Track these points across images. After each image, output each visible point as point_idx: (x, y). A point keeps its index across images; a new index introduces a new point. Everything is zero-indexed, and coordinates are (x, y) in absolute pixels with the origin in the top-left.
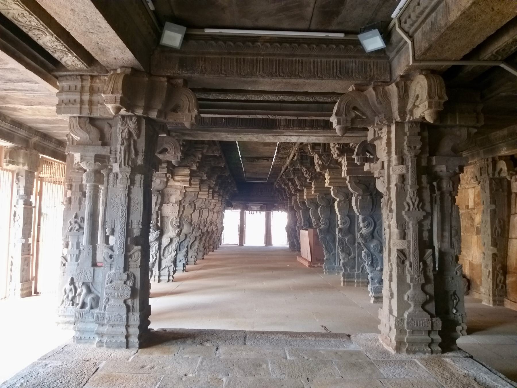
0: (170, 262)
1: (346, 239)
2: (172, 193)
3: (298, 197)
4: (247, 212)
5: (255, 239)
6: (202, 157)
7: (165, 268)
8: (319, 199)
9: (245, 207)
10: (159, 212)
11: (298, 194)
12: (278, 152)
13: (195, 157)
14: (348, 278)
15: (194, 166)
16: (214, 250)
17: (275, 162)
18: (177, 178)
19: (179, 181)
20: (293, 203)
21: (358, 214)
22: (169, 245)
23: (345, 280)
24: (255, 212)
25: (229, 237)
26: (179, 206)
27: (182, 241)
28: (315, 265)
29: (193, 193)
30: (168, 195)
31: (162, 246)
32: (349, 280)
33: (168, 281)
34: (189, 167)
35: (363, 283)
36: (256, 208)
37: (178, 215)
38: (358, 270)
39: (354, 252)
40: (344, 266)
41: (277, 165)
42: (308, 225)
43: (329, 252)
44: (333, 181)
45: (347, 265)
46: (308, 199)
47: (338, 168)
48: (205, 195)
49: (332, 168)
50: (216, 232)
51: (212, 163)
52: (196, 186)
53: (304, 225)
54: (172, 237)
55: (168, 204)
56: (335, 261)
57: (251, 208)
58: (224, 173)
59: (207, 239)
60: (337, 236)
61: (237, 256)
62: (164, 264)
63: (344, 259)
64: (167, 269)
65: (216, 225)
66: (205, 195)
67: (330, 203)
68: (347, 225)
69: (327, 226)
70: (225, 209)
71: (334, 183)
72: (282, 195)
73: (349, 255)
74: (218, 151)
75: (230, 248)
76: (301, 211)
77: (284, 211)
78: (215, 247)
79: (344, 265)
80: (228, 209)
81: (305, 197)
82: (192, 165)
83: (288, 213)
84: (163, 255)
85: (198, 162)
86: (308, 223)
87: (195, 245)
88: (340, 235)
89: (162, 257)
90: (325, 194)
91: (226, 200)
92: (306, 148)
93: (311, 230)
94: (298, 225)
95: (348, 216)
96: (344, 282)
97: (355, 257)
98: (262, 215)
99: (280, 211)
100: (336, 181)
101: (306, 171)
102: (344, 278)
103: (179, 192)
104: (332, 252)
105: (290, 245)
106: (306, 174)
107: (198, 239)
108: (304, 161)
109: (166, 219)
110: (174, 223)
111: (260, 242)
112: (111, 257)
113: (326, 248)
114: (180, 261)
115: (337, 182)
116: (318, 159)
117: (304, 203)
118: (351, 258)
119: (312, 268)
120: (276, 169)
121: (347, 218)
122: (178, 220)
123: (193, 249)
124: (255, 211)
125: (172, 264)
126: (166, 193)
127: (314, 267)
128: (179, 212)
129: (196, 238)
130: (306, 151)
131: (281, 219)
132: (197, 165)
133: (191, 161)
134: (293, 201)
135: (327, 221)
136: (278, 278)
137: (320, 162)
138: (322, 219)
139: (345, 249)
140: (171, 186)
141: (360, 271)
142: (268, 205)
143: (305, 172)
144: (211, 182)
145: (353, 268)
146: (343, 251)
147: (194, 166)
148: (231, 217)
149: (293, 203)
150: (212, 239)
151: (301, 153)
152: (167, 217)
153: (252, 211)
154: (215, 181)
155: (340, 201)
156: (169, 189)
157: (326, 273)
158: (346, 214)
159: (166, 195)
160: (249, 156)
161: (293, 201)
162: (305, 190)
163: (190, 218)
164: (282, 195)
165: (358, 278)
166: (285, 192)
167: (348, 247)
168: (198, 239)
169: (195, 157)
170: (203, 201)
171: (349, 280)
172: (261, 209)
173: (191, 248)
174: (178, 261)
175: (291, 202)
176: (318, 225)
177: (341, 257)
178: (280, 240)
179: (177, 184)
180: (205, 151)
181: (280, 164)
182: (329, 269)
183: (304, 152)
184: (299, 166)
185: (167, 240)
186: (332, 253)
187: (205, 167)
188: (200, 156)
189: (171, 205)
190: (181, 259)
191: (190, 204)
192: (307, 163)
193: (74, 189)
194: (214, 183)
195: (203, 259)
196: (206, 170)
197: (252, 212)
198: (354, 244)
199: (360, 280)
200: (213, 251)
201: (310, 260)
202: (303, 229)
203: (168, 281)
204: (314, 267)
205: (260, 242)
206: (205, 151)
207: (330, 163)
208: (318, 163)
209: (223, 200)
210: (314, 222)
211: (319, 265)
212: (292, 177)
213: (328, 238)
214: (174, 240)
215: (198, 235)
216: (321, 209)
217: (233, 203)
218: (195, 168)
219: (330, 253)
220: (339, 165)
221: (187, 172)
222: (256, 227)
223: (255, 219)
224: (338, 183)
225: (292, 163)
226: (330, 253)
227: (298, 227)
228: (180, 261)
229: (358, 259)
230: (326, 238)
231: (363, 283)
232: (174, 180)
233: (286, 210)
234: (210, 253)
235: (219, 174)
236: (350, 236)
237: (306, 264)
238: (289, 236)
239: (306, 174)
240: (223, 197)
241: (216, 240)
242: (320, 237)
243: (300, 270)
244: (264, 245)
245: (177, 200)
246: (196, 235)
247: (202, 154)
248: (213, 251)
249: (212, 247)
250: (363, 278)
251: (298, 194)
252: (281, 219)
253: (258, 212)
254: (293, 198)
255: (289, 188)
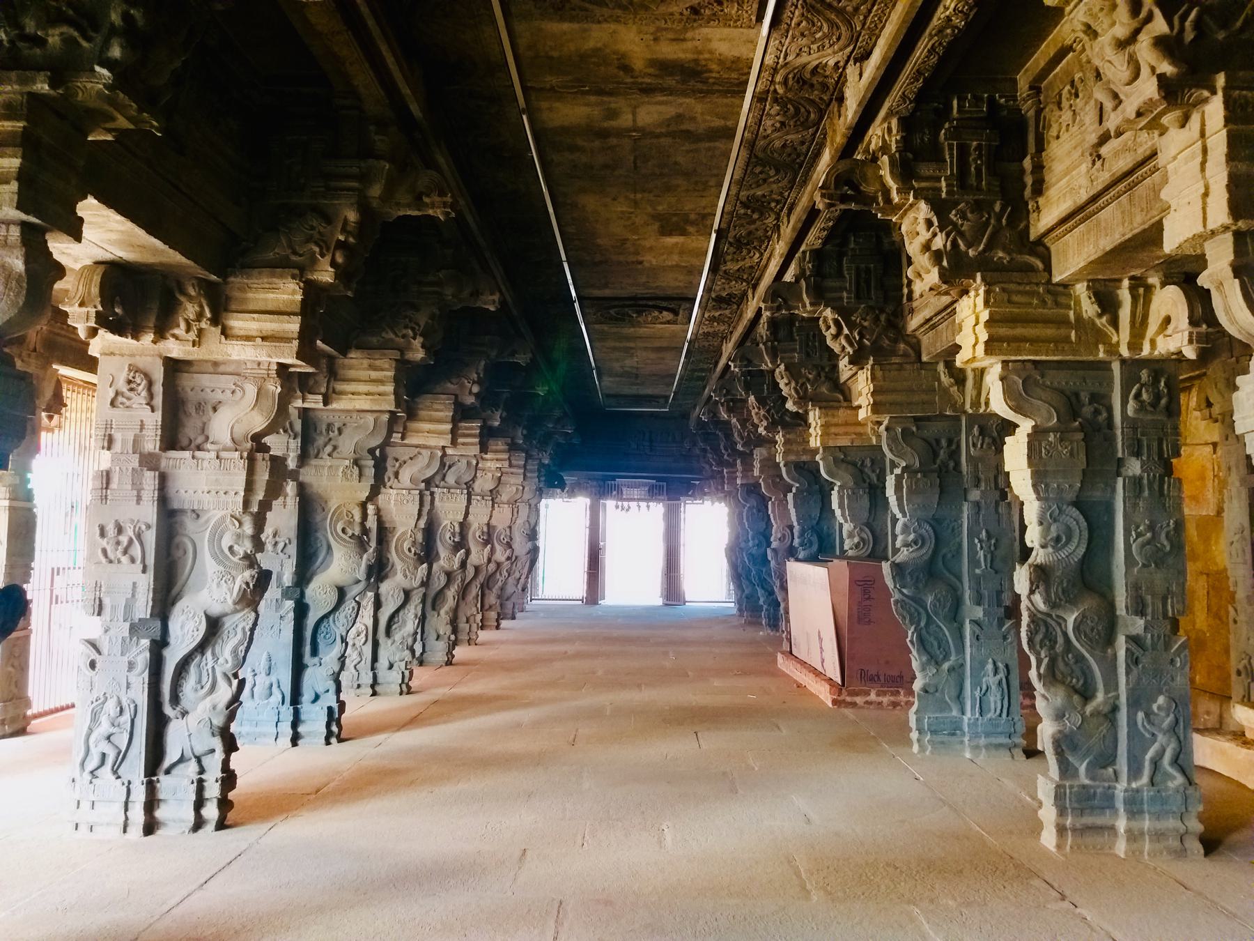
0: (206, 732)
1: (1071, 619)
2: (218, 396)
3: (780, 448)
4: (610, 504)
5: (633, 585)
6: (361, 224)
7: (182, 760)
8: (892, 440)
9: (603, 489)
10: (371, 508)
11: (779, 438)
12: (714, 269)
13: (328, 219)
14: (1082, 812)
15: (325, 263)
16: (504, 623)
17: (699, 324)
18: (238, 323)
19: (248, 338)
20: (756, 473)
21: (842, 521)
22: (201, 647)
23: (1069, 822)
24: (633, 504)
25: (558, 577)
26: (251, 461)
27: (326, 616)
28: (859, 700)
29: (370, 419)
30: (199, 407)
31: (167, 653)
32: (1088, 820)
33: (401, 694)
34: (301, 271)
35: (1158, 836)
36: (636, 493)
37: (246, 504)
38: (1135, 772)
39: (1111, 684)
40: (1059, 753)
41: (707, 335)
42: (815, 547)
43: (934, 660)
44: (1003, 331)
45: (1074, 748)
46: (825, 448)
47: (1031, 269)
48: (441, 433)
49: (999, 268)
50: (506, 565)
51: (449, 291)
52: (381, 388)
53: (801, 545)
54: (216, 610)
55: (199, 448)
56: (959, 697)
57: (620, 492)
58: (513, 354)
59: (476, 590)
60: (1024, 603)
61: (570, 648)
62: (177, 740)
63: (1059, 716)
64: (192, 767)
65: (509, 545)
66: (441, 433)
67: (935, 454)
68: (1076, 549)
69: (927, 551)
70: (540, 493)
71: (1009, 340)
72: (716, 450)
73: (1086, 694)
74: (442, 194)
75: (557, 612)
76: (790, 496)
77: (720, 500)
78: (509, 610)
79: (1063, 744)
80: (552, 496)
81: (815, 442)
82: (314, 261)
83: (730, 506)
84: (175, 699)
85: (341, 245)
86: (815, 539)
87: (404, 622)
88: (1038, 599)
89: (168, 710)
90: (916, 419)
91: (541, 465)
92: (870, 173)
93: (840, 565)
94: (774, 545)
95: (1077, 504)
96: (1061, 830)
97: (1115, 709)
98: (656, 511)
99: (708, 503)
100: (1019, 331)
101: (836, 322)
102: (1062, 812)
103: (251, 390)
104: (946, 658)
105: (739, 602)
106: (836, 337)
107: (416, 599)
108: (831, 283)
109: (190, 525)
110: (226, 542)
111: (649, 594)
112: (93, 665)
113: (922, 643)
114: (317, 698)
115: (1024, 339)
116: (929, 223)
117: (806, 470)
118: (1096, 713)
119: (848, 712)
120: (704, 351)
121: (1075, 512)
122: (248, 529)
123: (398, 636)
124: (633, 500)
125: (217, 744)
126: (192, 397)
127: (854, 705)
128: (249, 487)
129: (407, 594)
130: (869, 189)
131: (709, 523)
132: (340, 259)
133: (309, 240)
134: (757, 464)
135: (927, 530)
136: (726, 782)
137: (939, 243)
138: (902, 521)
139: (1061, 665)
140: (216, 364)
141: (1145, 779)
142: (673, 481)
143: (833, 330)
144: (462, 386)
145: (1106, 759)
146: (1051, 677)
147: (325, 263)
148: (563, 519)
149: (756, 473)
150: (495, 590)
151: (844, 199)
152: (197, 515)
153: (622, 500)
154: (479, 382)
155: (1036, 436)
156: (206, 380)
157: (922, 749)
158: (1070, 496)
159: (191, 409)
160: (607, 293)
161: (757, 464)
162: (814, 417)
163: (358, 518)
164: (716, 450)
165: (1134, 806)
166: (729, 436)
167: (1080, 659)
168: (416, 599)
169: (328, 219)
170: (432, 457)
171: (1088, 820)
172: (653, 493)
173: (388, 633)
174: (307, 696)
175: (748, 467)
176: (876, 549)
177: (1040, 705)
178: (710, 585)
179: (237, 352)
180: (376, 191)
181: (715, 335)
182: (934, 732)
183: (860, 197)
184: (805, 308)
185: (191, 625)
186: (946, 666)
187: (416, 308)
188: (352, 216)
189: (208, 456)
190: (320, 690)
191: (356, 462)
192: (842, 289)
193: (117, 447)
194: (476, 389)
195: (449, 663)
196: (423, 319)
197: (626, 504)
198: (1110, 640)
199: (1147, 824)
200: (498, 627)
201: (834, 672)
202: (797, 560)
203: (401, 694)
204: (854, 705)
205: (649, 594)
206: (376, 191)
207: (989, 247)
208: (927, 247)
209: (533, 465)
210: (851, 535)
211: (873, 697)
212: (767, 365)
213: (929, 600)
214: (228, 623)
215: (416, 583)
216: (899, 479)
217: (569, 479)
218: (325, 275)
219: (938, 664)
220: (1033, 253)
221: (289, 292)
222: (635, 551)
223: (634, 523)
224: (1033, 341)
225: (779, 292)
226: (938, 664)
227: (774, 550)
228: (317, 698)
229: (1132, 723)
230: (920, 602)
231: (1158, 836)
232: (225, 333)
233: (727, 496)
234: (483, 635)
235: (493, 354)
236: (1089, 603)
237: (824, 694)
238: (739, 575)
239: (836, 337)
240: (528, 457)
241: (510, 589)
242: (896, 596)
243: (787, 708)
244: (658, 601)
245: (240, 431)
246: (406, 584)
247: (364, 208)
248: (498, 627)
249: (493, 615)
250: (1157, 816)
251: (779, 438)
252: (709, 523)
253: (643, 504)
254: (759, 453)
255: (745, 421)
